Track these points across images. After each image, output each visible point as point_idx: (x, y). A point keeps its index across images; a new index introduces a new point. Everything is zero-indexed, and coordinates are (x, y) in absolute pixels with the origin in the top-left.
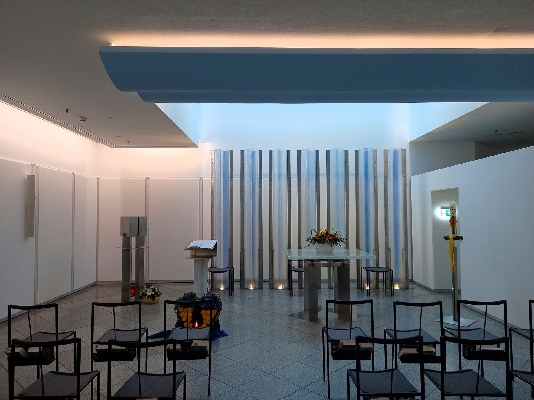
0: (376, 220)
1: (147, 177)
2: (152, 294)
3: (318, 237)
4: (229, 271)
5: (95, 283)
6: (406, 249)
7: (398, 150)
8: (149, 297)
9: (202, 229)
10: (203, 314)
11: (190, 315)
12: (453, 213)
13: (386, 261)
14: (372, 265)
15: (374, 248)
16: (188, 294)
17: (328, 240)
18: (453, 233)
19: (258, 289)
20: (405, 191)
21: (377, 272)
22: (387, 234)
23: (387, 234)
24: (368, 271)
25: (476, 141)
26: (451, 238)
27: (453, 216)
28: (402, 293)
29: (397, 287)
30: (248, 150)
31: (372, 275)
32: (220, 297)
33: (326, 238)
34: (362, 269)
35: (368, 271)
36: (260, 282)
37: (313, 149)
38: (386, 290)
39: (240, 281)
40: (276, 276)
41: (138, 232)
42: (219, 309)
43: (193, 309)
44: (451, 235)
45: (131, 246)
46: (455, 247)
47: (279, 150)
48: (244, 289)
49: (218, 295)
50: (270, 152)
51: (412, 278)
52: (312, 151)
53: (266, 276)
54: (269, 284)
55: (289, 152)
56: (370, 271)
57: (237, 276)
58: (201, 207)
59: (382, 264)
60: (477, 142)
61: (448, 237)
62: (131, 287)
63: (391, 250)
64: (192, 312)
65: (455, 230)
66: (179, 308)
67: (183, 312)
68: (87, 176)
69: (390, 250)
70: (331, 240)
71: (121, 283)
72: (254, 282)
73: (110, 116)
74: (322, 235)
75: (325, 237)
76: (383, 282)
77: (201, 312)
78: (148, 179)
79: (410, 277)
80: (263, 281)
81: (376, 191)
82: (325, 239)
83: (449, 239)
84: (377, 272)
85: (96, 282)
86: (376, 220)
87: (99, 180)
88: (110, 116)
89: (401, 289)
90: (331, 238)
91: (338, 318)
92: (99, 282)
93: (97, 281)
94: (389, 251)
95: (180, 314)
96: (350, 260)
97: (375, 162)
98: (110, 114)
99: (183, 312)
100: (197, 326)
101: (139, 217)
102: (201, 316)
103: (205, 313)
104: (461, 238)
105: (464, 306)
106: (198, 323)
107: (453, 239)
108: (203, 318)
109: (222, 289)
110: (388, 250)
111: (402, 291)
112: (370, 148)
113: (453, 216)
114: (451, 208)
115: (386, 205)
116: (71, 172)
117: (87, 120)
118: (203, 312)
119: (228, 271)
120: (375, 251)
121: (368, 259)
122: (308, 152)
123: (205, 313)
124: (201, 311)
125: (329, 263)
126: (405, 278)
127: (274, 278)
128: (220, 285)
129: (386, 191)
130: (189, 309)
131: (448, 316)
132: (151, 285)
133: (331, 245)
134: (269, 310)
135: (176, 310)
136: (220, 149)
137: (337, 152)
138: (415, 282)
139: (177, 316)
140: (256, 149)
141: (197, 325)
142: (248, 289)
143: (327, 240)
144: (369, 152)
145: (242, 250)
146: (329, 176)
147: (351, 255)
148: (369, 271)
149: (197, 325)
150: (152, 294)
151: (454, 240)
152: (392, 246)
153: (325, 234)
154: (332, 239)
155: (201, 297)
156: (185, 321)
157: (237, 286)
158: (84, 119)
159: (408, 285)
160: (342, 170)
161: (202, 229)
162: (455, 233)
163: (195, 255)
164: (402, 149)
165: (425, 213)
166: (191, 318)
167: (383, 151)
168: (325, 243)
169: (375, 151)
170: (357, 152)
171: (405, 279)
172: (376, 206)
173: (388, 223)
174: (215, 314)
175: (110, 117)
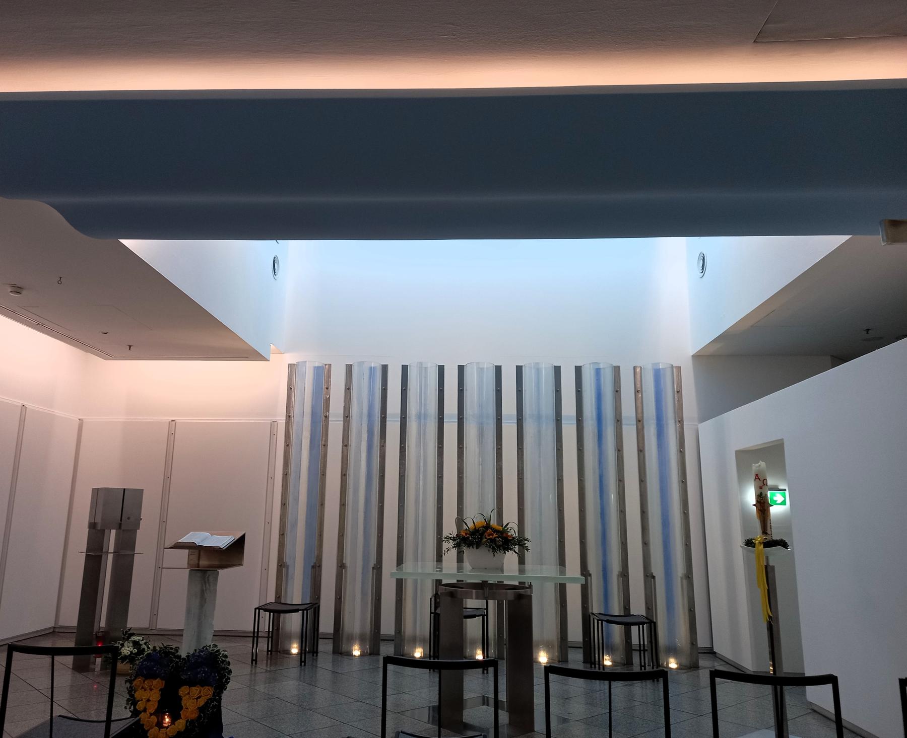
0: (621, 511)
1: (173, 418)
2: (131, 652)
3: (466, 534)
4: (303, 610)
5: (51, 631)
6: (689, 577)
7: (662, 369)
8: (125, 658)
9: (270, 524)
10: (184, 696)
11: (155, 696)
12: (761, 488)
13: (646, 603)
14: (616, 609)
15: (619, 572)
16: (160, 648)
17: (488, 539)
18: (765, 532)
19: (370, 654)
20: (681, 451)
21: (628, 626)
22: (645, 543)
23: (645, 544)
24: (600, 622)
25: (832, 356)
26: (760, 543)
27: (761, 494)
28: (684, 677)
29: (673, 664)
30: (361, 364)
31: (617, 631)
32: (226, 656)
33: (484, 537)
34: (596, 621)
35: (600, 622)
36: (374, 640)
37: (488, 365)
38: (271, 654)
39: (332, 637)
40: (408, 629)
41: (121, 521)
42: (220, 686)
43: (164, 682)
44: (759, 537)
45: (104, 550)
46: (771, 564)
47: (421, 363)
48: (341, 654)
49: (223, 652)
50: (405, 369)
51: (709, 646)
52: (486, 368)
53: (388, 627)
54: (393, 647)
55: (441, 369)
56: (605, 621)
57: (326, 625)
58: (271, 478)
59: (638, 608)
60: (832, 356)
61: (752, 539)
62: (97, 637)
63: (656, 577)
64: (160, 690)
65: (769, 525)
66: (134, 680)
67: (143, 688)
68: (58, 412)
69: (654, 577)
70: (493, 541)
71: (75, 631)
72: (362, 640)
73: (60, 281)
74: (475, 528)
75: (482, 534)
76: (638, 652)
77: (180, 690)
78: (174, 422)
79: (702, 642)
80: (382, 638)
81: (619, 450)
82: (481, 539)
83: (755, 544)
84: (628, 626)
85: (54, 628)
86: (622, 512)
87: (82, 423)
88: (60, 281)
89: (681, 667)
90: (495, 535)
91: (508, 723)
92: (61, 627)
93: (57, 626)
94: (653, 580)
95: (135, 693)
96: (567, 584)
97: (617, 392)
98: (60, 278)
99: (143, 688)
100: (168, 723)
101: (124, 489)
102: (180, 699)
103: (189, 693)
104: (783, 544)
105: (812, 709)
106: (170, 717)
107: (762, 546)
108: (183, 705)
109: (356, 652)
110: (649, 577)
111: (684, 671)
112: (605, 365)
113: (761, 494)
114: (757, 475)
115: (642, 481)
116: (19, 402)
117: (24, 292)
118: (183, 691)
119: (301, 610)
120: (621, 579)
121: (563, 582)
122: (480, 370)
123: (189, 693)
124: (180, 688)
125: (483, 589)
126: (689, 642)
127: (404, 632)
128: (290, 643)
129: (641, 451)
130: (155, 682)
131: (767, 730)
132: (133, 634)
133: (493, 549)
134: (365, 699)
135: (128, 685)
136: (306, 361)
137: (538, 371)
138: (717, 655)
139: (128, 697)
140: (377, 364)
141: (167, 720)
142: (349, 654)
143: (484, 540)
144: (602, 370)
145: (341, 566)
146: (581, 448)
147: (569, 574)
148: (602, 621)
149: (167, 720)
150: (131, 652)
151: (764, 547)
152: (658, 569)
153: (483, 527)
154: (496, 537)
155: (187, 656)
156: (142, 709)
157: (325, 647)
158: (18, 290)
159: (697, 660)
160: (548, 409)
161: (270, 524)
162: (769, 532)
163: (198, 564)
164: (672, 365)
165: (726, 500)
166: (157, 703)
167: (632, 369)
168: (480, 546)
169: (617, 370)
170: (578, 370)
171: (689, 646)
172: (621, 481)
173: (648, 519)
174: (209, 697)
175: (60, 282)
